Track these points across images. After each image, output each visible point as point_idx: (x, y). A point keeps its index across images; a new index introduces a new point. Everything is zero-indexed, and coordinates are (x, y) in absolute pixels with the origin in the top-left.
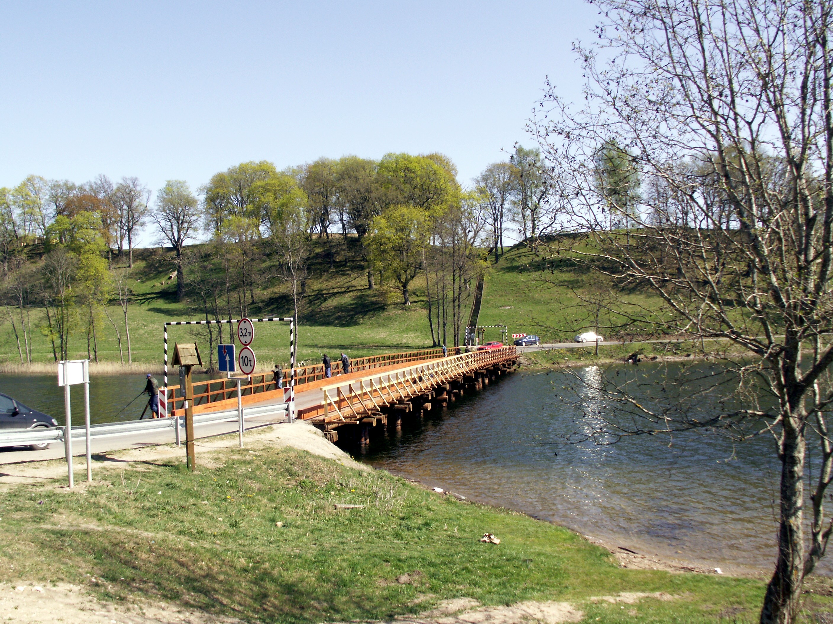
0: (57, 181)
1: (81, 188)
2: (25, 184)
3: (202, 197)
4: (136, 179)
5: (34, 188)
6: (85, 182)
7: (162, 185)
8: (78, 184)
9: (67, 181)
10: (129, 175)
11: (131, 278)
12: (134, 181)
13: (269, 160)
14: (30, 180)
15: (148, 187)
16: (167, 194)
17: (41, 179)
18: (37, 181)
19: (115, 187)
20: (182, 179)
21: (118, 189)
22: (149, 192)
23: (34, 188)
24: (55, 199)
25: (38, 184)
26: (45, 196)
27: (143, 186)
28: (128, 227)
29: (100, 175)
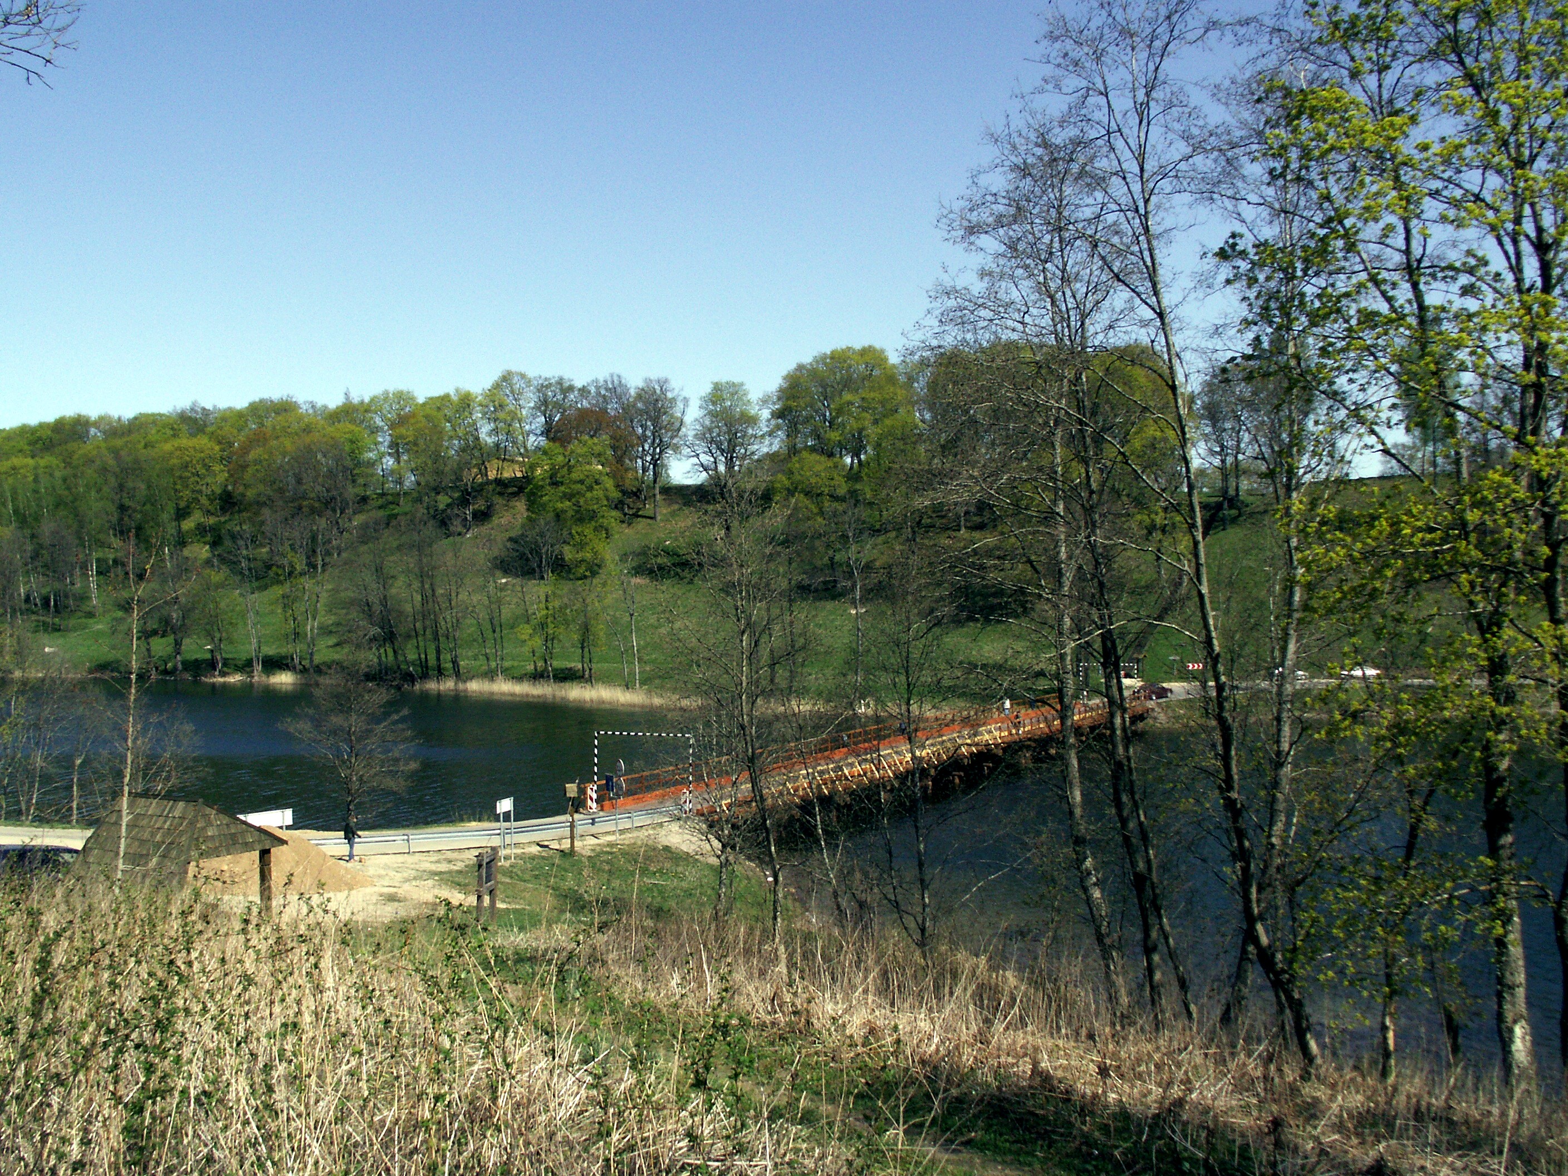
0: (546, 379)
1: (584, 391)
2: (497, 386)
3: (765, 414)
4: (666, 381)
5: (512, 392)
6: (589, 380)
7: (707, 389)
8: (579, 384)
9: (561, 379)
10: (654, 375)
11: (1152, 274)
12: (663, 383)
13: (878, 345)
14: (506, 378)
15: (685, 394)
16: (714, 403)
17: (523, 376)
18: (515, 379)
19: (633, 392)
20: (736, 380)
21: (639, 397)
22: (686, 400)
23: (512, 392)
24: (544, 405)
25: (518, 384)
26: (530, 400)
27: (676, 392)
28: (653, 455)
29: (612, 376)
